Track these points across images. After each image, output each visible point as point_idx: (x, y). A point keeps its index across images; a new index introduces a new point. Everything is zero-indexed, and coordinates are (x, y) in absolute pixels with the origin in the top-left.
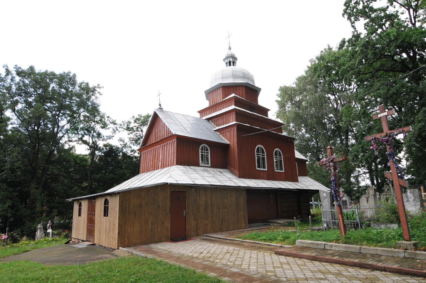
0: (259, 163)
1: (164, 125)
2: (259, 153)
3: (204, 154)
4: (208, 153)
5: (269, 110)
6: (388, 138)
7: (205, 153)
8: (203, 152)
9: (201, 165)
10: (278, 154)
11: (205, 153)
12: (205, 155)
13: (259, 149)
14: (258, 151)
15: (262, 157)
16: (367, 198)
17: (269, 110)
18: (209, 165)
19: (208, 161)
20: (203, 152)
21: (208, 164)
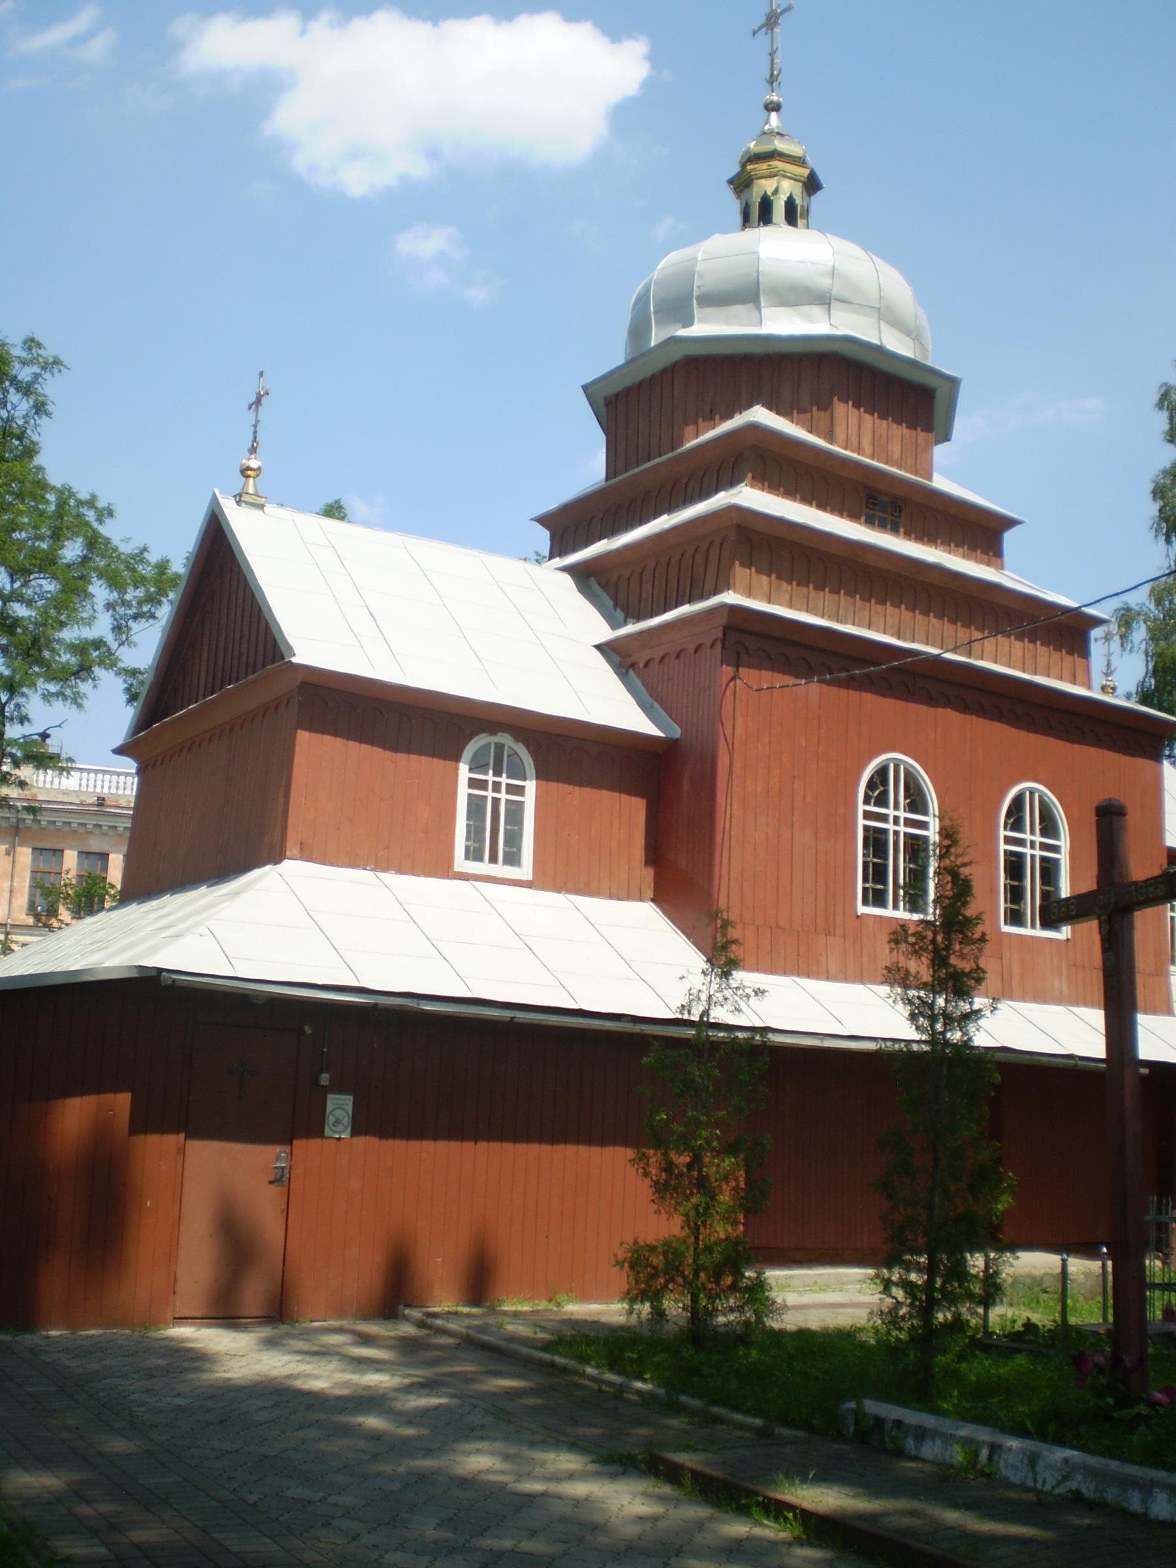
0: (475, 833)
1: (262, 639)
2: (886, 806)
3: (490, 794)
4: (520, 790)
5: (1010, 523)
6: (38, 370)
7: (497, 787)
8: (482, 785)
9: (461, 863)
10: (896, 791)
11: (497, 787)
12: (496, 801)
13: (885, 782)
14: (1015, 817)
15: (1043, 859)
16: (216, 1345)
17: (1010, 523)
18: (525, 870)
19: (514, 839)
20: (482, 785)
21: (513, 859)
